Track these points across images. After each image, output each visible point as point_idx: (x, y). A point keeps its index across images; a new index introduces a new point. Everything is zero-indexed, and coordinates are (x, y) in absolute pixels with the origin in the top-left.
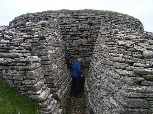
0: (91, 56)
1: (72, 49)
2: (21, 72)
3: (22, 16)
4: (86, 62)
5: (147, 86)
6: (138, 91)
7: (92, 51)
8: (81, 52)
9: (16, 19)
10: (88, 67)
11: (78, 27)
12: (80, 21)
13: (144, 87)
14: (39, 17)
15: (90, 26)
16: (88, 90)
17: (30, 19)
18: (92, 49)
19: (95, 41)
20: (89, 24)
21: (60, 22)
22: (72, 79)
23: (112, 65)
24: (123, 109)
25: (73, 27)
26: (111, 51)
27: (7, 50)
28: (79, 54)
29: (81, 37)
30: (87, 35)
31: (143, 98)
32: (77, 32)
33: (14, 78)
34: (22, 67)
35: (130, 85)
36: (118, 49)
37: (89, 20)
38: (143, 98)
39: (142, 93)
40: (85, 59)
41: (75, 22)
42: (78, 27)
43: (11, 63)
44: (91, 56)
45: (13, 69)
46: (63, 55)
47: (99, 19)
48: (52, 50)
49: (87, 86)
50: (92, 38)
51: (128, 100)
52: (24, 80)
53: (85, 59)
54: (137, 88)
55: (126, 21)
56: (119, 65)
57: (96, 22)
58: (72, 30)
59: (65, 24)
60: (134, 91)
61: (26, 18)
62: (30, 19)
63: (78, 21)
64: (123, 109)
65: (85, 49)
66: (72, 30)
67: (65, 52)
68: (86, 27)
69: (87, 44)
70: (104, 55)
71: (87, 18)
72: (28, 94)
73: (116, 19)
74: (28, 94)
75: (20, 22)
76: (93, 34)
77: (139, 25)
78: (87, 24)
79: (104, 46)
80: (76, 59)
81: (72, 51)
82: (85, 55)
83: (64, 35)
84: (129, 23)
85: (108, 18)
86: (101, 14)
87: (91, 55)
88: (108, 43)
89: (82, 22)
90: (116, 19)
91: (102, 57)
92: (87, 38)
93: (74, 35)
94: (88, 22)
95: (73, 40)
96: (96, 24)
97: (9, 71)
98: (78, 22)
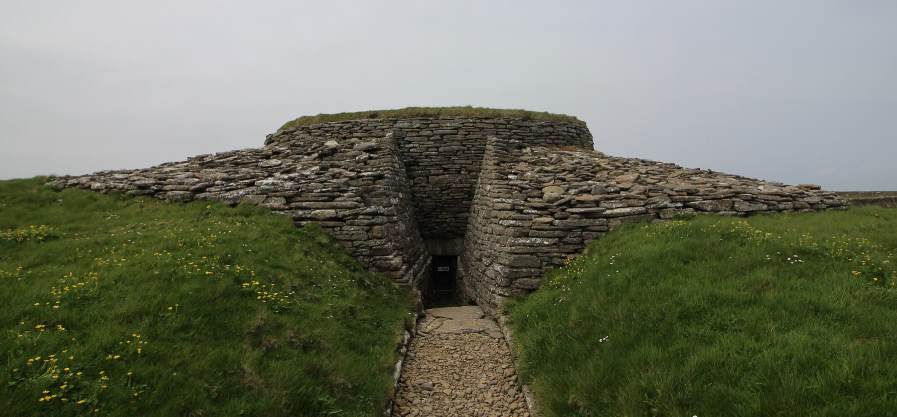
0: (468, 212)
1: (427, 198)
2: (366, 228)
3: (306, 120)
4: (459, 225)
5: (537, 237)
6: (524, 245)
7: (471, 200)
8: (446, 202)
9: (291, 129)
10: (462, 236)
11: (438, 148)
12: (442, 135)
13: (533, 239)
14: (350, 128)
15: (465, 145)
16: (464, 273)
17: (327, 131)
18: (470, 194)
19: (476, 177)
20: (461, 141)
21: (398, 140)
22: (429, 261)
23: (496, 217)
24: (507, 270)
25: (428, 148)
26: (497, 195)
27: (332, 198)
28: (443, 207)
29: (445, 170)
30: (458, 166)
31: (532, 254)
32: (436, 160)
33: (354, 237)
34: (366, 221)
35: (516, 237)
36: (680, 229)
37: (461, 132)
38: (532, 254)
39: (531, 246)
40: (456, 218)
41: (432, 138)
42: (438, 148)
43: (349, 215)
44: (468, 212)
45: (352, 224)
46: (410, 210)
47: (481, 129)
48: (395, 198)
49: (461, 269)
50: (469, 172)
51: (513, 257)
52: (369, 239)
53: (456, 218)
54: (524, 241)
55: (543, 130)
56: (503, 214)
57: (477, 137)
58: (427, 156)
59: (410, 142)
60: (519, 245)
61: (319, 128)
62: (327, 131)
63: (437, 135)
64: (507, 270)
65: (458, 196)
66: (427, 156)
67: (412, 203)
68: (456, 148)
69: (459, 186)
70: (488, 203)
71: (457, 129)
72: (374, 260)
73: (519, 127)
74: (374, 260)
75: (301, 136)
76: (470, 162)
77: (577, 134)
78: (458, 141)
79: (488, 187)
80: (437, 218)
81: (428, 200)
82: (457, 209)
83: (411, 165)
84: (551, 133)
85: (501, 126)
86: (486, 119)
87: (469, 208)
88: (494, 182)
89: (448, 136)
90: (519, 127)
91: (485, 207)
92: (459, 172)
93: (431, 166)
94: (459, 137)
95: (428, 177)
96: (476, 140)
97: (345, 228)
98: (439, 137)
